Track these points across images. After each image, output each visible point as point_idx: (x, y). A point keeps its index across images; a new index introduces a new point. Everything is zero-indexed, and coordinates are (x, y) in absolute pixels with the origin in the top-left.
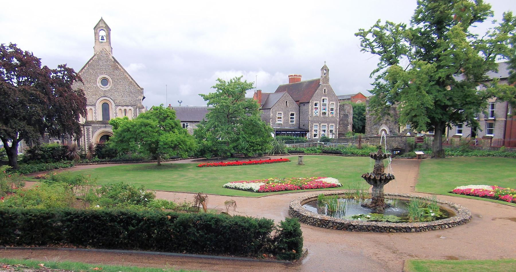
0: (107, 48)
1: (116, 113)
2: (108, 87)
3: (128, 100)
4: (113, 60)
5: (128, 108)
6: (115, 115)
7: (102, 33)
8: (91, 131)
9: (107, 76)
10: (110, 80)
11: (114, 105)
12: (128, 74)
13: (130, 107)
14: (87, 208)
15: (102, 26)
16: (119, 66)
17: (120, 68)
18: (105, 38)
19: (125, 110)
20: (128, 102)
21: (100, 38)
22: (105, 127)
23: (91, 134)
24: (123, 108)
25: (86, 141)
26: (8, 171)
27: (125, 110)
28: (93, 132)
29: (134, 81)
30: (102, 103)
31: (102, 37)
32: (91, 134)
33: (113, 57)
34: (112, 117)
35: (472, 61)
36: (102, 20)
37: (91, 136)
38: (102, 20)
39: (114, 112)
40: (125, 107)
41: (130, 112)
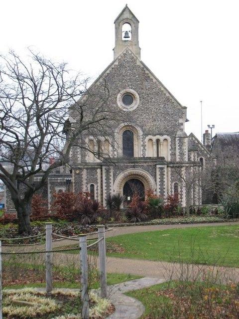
0: (133, 49)
1: (144, 146)
2: (134, 106)
3: (161, 124)
4: (142, 66)
5: (161, 138)
6: (142, 148)
7: (126, 28)
8: (112, 174)
9: (132, 91)
10: (137, 96)
11: (141, 133)
12: (163, 86)
13: (165, 137)
14: (173, 265)
15: (127, 18)
16: (150, 75)
17: (151, 77)
18: (130, 34)
19: (158, 141)
20: (162, 127)
21: (123, 35)
22: (134, 167)
23: (112, 178)
24: (154, 138)
25: (104, 188)
26: (9, 234)
27: (158, 141)
28: (115, 176)
29: (173, 97)
30: (122, 132)
31: (126, 33)
32: (112, 178)
33: (141, 62)
34: (138, 153)
35: (63, 111)
36: (126, 8)
37: (112, 181)
38: (126, 8)
39: (142, 143)
40: (158, 137)
41: (165, 143)
